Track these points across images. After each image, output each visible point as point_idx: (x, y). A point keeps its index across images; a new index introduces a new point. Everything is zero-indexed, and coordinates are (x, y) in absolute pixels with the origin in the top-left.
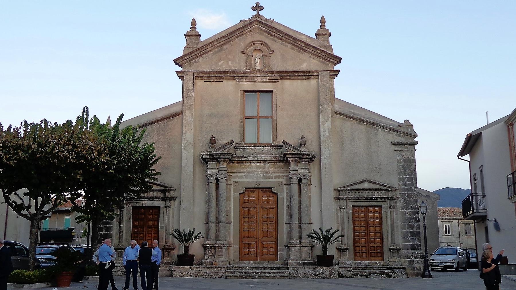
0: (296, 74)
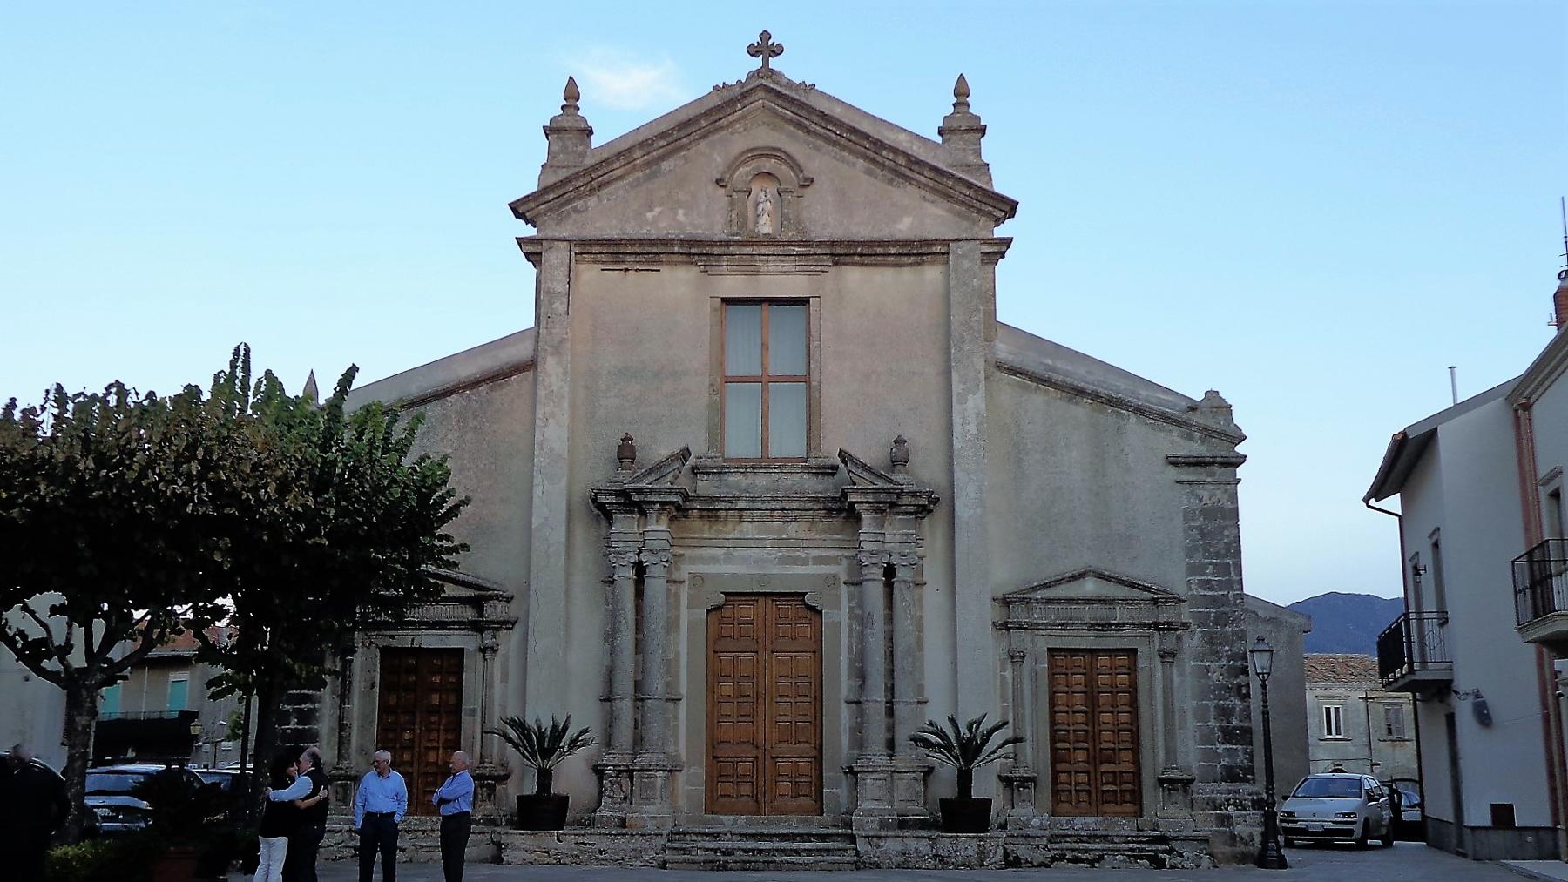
0: (879, 250)
